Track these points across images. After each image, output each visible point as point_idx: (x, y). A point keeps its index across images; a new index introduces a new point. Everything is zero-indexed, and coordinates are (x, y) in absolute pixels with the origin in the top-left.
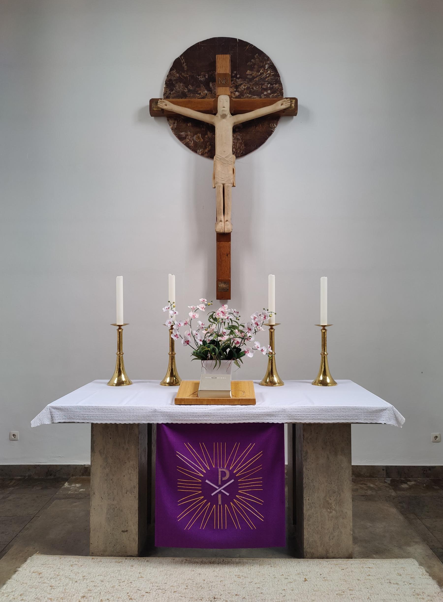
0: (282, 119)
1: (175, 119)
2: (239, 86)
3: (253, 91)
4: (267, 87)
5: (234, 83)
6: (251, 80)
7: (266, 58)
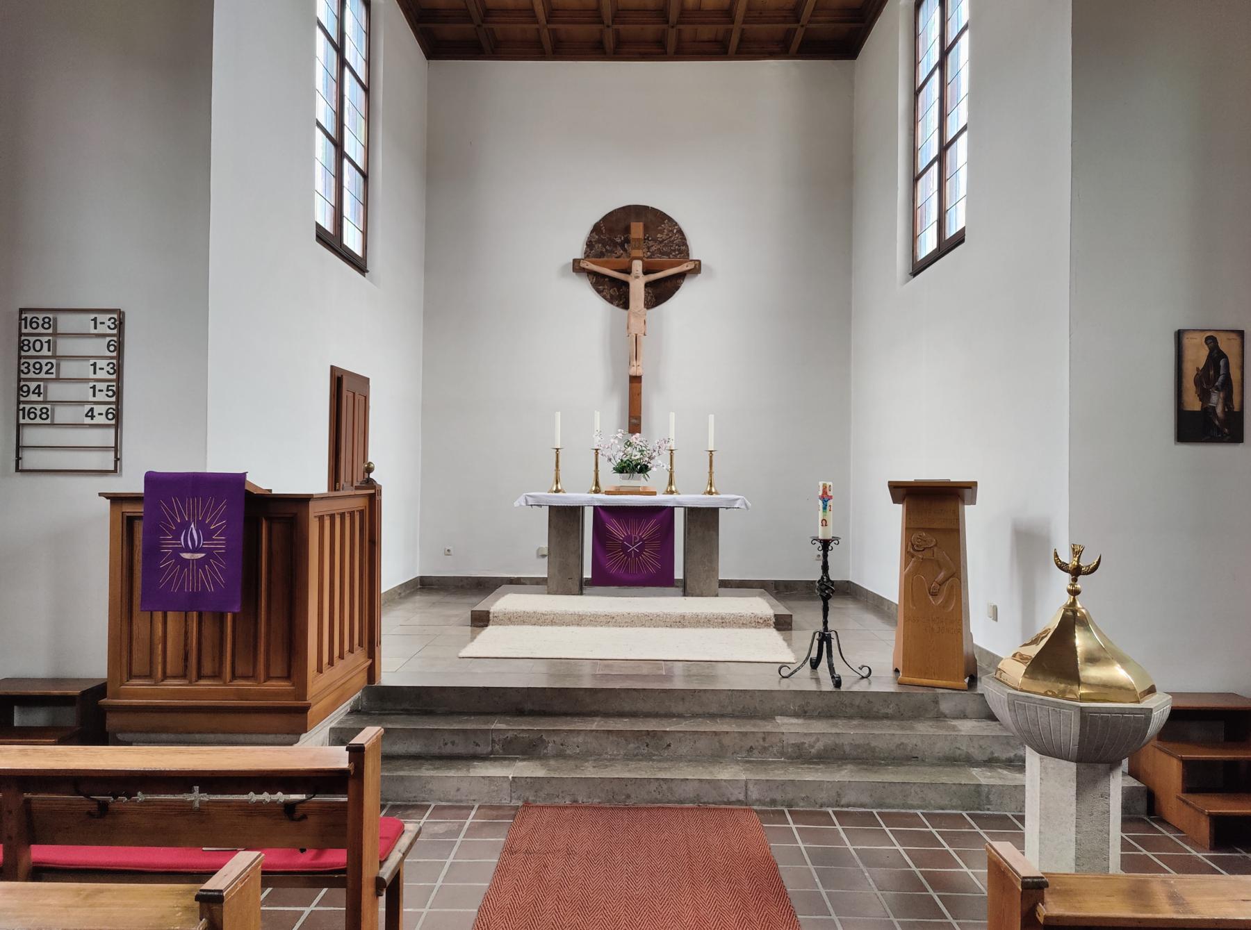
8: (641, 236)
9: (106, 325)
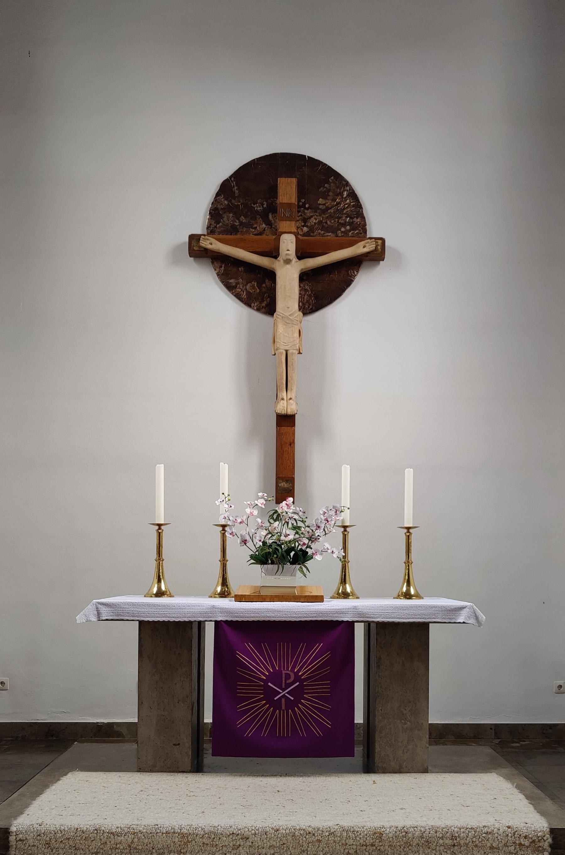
0: (364, 264)
1: (222, 262)
2: (308, 219)
3: (326, 226)
4: (346, 222)
5: (301, 215)
6: (324, 211)
7: (344, 182)
8: (294, 200)
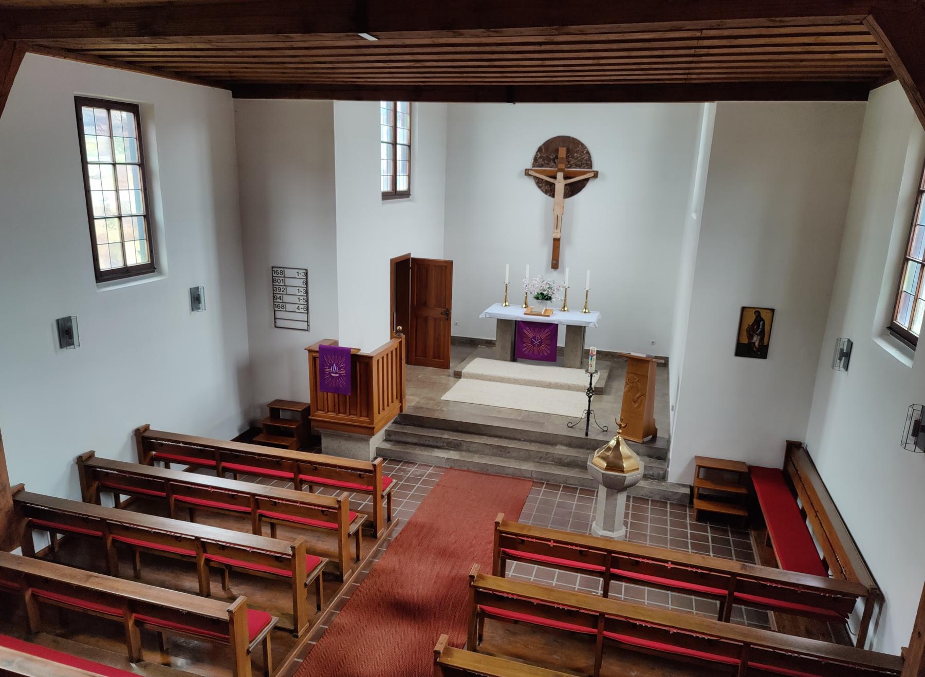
9: (302, 275)
